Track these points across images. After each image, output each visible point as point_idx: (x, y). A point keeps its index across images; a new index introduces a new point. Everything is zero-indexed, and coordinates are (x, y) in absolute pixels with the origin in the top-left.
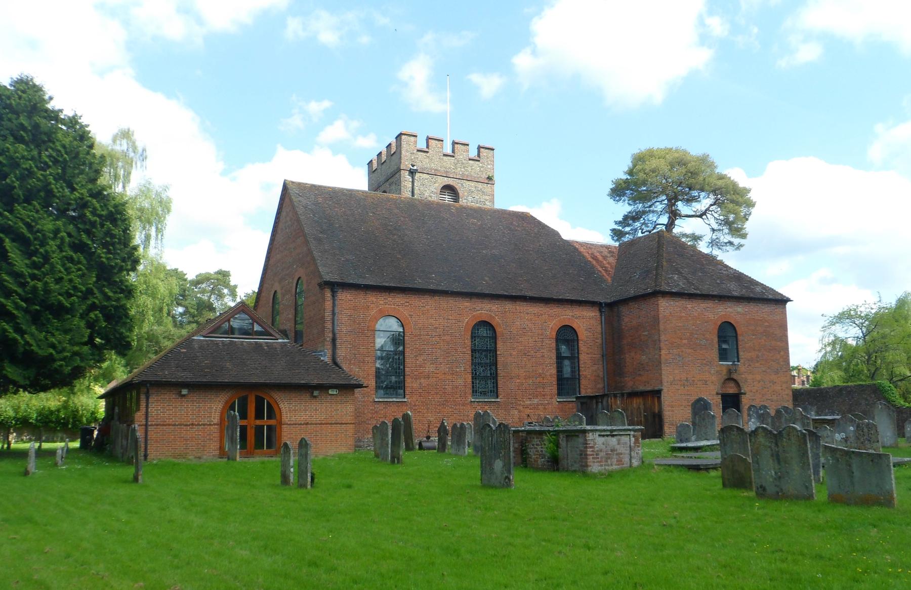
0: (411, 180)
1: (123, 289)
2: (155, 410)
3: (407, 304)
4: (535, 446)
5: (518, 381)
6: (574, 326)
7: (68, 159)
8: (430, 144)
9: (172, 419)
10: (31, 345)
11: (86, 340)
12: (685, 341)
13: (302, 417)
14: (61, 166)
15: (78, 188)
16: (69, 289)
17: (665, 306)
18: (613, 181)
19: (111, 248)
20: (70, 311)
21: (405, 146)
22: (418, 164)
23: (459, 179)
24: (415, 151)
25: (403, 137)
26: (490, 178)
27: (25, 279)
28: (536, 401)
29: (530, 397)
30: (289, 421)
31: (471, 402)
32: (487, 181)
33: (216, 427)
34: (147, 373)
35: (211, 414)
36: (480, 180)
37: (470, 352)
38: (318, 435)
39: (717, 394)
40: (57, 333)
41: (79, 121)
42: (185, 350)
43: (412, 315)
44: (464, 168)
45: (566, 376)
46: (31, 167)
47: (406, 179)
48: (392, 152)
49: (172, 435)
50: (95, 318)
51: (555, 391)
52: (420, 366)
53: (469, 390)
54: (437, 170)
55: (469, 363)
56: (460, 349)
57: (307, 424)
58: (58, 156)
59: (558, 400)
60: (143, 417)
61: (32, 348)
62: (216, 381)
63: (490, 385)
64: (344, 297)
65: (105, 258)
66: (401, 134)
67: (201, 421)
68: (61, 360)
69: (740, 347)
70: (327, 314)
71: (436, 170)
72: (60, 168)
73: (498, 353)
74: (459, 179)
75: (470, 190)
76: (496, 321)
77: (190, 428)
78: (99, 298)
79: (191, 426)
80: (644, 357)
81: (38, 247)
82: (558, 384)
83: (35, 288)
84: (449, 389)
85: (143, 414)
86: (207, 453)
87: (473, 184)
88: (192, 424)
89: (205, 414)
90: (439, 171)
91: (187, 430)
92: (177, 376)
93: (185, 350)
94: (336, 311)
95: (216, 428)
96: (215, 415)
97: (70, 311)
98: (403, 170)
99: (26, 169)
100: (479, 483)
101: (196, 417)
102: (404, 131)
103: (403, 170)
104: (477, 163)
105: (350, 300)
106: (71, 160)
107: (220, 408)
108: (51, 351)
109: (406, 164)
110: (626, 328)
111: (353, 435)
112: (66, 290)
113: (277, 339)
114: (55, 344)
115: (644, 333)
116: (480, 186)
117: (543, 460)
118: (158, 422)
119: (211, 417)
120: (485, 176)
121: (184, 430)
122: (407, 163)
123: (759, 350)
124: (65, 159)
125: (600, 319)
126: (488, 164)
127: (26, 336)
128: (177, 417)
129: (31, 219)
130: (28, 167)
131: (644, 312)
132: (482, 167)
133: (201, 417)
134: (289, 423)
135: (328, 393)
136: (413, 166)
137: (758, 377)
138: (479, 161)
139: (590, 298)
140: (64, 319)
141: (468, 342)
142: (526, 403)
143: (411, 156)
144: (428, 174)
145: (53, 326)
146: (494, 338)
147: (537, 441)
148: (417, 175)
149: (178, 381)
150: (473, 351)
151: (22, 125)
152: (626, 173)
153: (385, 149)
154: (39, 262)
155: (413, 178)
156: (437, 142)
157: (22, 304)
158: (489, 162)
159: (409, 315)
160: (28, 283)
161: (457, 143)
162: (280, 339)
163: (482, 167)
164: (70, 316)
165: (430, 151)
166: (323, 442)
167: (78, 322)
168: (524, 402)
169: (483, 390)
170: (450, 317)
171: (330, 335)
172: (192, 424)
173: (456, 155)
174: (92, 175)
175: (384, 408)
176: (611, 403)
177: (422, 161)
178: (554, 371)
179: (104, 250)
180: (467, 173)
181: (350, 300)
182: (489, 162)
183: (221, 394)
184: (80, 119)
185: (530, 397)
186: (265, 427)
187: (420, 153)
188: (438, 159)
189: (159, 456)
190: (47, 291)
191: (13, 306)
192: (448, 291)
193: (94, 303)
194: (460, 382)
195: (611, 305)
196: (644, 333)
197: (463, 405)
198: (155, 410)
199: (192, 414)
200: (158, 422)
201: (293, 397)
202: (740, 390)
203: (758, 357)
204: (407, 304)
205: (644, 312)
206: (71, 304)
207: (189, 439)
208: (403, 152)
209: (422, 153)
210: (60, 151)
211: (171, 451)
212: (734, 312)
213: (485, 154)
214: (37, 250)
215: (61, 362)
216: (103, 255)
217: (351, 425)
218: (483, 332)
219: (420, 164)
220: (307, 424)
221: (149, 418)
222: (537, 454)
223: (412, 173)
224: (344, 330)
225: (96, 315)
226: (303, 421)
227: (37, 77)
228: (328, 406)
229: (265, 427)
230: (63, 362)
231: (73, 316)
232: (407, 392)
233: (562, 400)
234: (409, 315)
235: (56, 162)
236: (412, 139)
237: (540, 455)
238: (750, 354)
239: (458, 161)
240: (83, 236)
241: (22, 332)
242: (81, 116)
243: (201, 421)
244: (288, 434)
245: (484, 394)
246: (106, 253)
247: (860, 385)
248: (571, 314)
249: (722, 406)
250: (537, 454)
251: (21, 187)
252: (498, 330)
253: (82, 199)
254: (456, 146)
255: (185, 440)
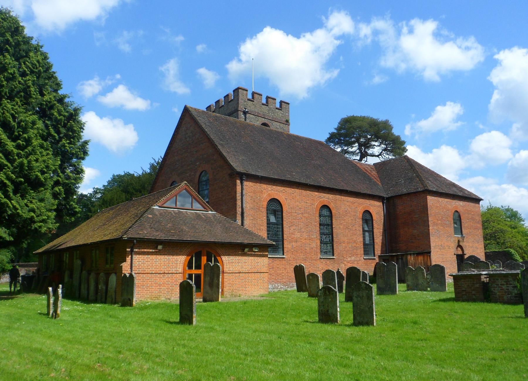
0: (244, 118)
1: (79, 171)
2: (137, 261)
3: (284, 191)
4: (500, 285)
5: (344, 245)
6: (371, 211)
7: (42, 71)
8: (255, 96)
9: (150, 269)
10: (17, 209)
11: (56, 207)
12: (440, 222)
13: (237, 269)
14: (36, 76)
15: (46, 94)
16: (44, 168)
17: (431, 200)
18: (329, 133)
19: (72, 140)
20: (42, 185)
21: (241, 96)
22: (248, 108)
23: (271, 120)
24: (246, 100)
25: (240, 90)
26: (287, 121)
27: (13, 157)
28: (353, 258)
29: (350, 255)
30: (228, 270)
31: (320, 258)
32: (285, 123)
33: (180, 275)
34: (131, 232)
35: (177, 265)
36: (282, 122)
37: (318, 225)
38: (246, 281)
39: (455, 254)
40: (34, 201)
41: (41, 49)
42: (151, 216)
43: (287, 199)
44: (273, 113)
45: (366, 243)
46: (14, 73)
47: (241, 117)
48: (229, 100)
49: (149, 282)
50: (59, 192)
51: (363, 252)
52: (292, 234)
53: (319, 251)
54: (259, 113)
55: (319, 233)
56: (313, 223)
57: (240, 273)
58: (34, 68)
59: (365, 258)
60: (129, 267)
61: (18, 211)
62: (182, 239)
63: (329, 248)
64: (248, 184)
65: (69, 147)
66: (238, 89)
67: (170, 270)
68: (41, 222)
69: (462, 226)
70: (238, 195)
71: (258, 113)
72: (35, 77)
73: (333, 226)
74: (271, 120)
75: (276, 127)
76: (331, 206)
77: (163, 276)
78: (62, 177)
79: (163, 275)
80: (416, 231)
81: (21, 133)
82: (364, 248)
83: (22, 165)
84: (308, 249)
85: (128, 265)
86: (174, 295)
87: (278, 124)
88: (164, 273)
89: (173, 265)
90: (260, 114)
91: (161, 278)
92: (154, 235)
93: (151, 216)
94: (244, 193)
95: (180, 276)
96: (180, 265)
97: (42, 185)
98: (240, 111)
99: (11, 74)
100: (524, 315)
101: (167, 267)
102: (241, 86)
103: (240, 111)
104: (280, 111)
105: (251, 186)
106: (43, 72)
107: (183, 260)
108: (32, 214)
109: (241, 107)
110: (401, 213)
111: (267, 281)
112: (42, 168)
113: (208, 211)
114: (35, 209)
115: (415, 216)
116: (282, 125)
117: (509, 296)
118: (139, 271)
119: (177, 267)
120: (284, 120)
121: (158, 278)
122: (242, 107)
123: (470, 229)
124: (40, 71)
125: (382, 207)
126: (286, 113)
127: (12, 201)
128: (153, 267)
129: (15, 112)
130: (13, 73)
131: (415, 203)
132: (283, 114)
133: (170, 267)
134: (228, 272)
135: (252, 250)
136: (245, 109)
137: (471, 245)
138: (281, 110)
139: (377, 194)
140: (39, 191)
141: (318, 219)
142: (348, 259)
143: (244, 103)
144: (254, 115)
145: (30, 195)
146: (331, 216)
147: (502, 282)
148: (248, 115)
149: (156, 239)
150: (320, 225)
151: (8, 40)
152: (336, 129)
153: (223, 99)
154: (23, 144)
155: (245, 117)
156: (258, 96)
157: (12, 176)
158: (287, 111)
159: (285, 199)
160: (15, 159)
161: (270, 98)
162: (210, 211)
163: (283, 114)
164: (43, 189)
165: (255, 100)
166: (250, 286)
167: (48, 195)
168: (347, 259)
169: (326, 251)
170: (308, 202)
171: (240, 210)
172: (164, 273)
173: (269, 105)
174: (55, 87)
175: (272, 262)
176: (409, 259)
177: (250, 107)
178: (362, 239)
179: (68, 141)
180: (275, 117)
181: (251, 186)
182: (287, 111)
183: (184, 250)
184: (41, 48)
185: (350, 255)
186: (194, 275)
187: (249, 102)
188: (259, 107)
189: (141, 298)
190: (30, 168)
191: (5, 177)
192: (307, 184)
193: (58, 180)
194: (314, 245)
195: (388, 199)
196: (415, 216)
197: (316, 260)
198: (137, 261)
199: (138, 265)
200: (139, 271)
201: (231, 253)
202: (464, 253)
203: (470, 232)
204: (284, 191)
205: (415, 203)
206: (45, 179)
207: (162, 285)
208: (240, 100)
209: (250, 102)
210: (36, 65)
211: (149, 294)
212: (460, 205)
213: (284, 106)
214: (20, 135)
215: (41, 224)
216: (67, 145)
217: (266, 274)
218: (325, 212)
219: (249, 109)
220: (240, 273)
221: (133, 268)
222: (502, 292)
223: (245, 113)
224: (248, 206)
225: (59, 190)
226: (237, 270)
227: (13, 11)
228: (252, 260)
229: (194, 275)
230: (42, 224)
231: (45, 189)
232: (285, 251)
233: (366, 258)
234: (285, 199)
235: (32, 72)
236: (245, 92)
237: (505, 292)
238: (467, 231)
239: (270, 109)
240: (51, 130)
241: (10, 199)
242: (42, 46)
243: (170, 270)
244: (228, 280)
245: (326, 253)
246: (68, 143)
247: (495, 251)
248: (369, 203)
249: (457, 262)
250: (502, 292)
251: (7, 86)
252: (333, 212)
253: (50, 102)
254: (269, 99)
255: (159, 285)
